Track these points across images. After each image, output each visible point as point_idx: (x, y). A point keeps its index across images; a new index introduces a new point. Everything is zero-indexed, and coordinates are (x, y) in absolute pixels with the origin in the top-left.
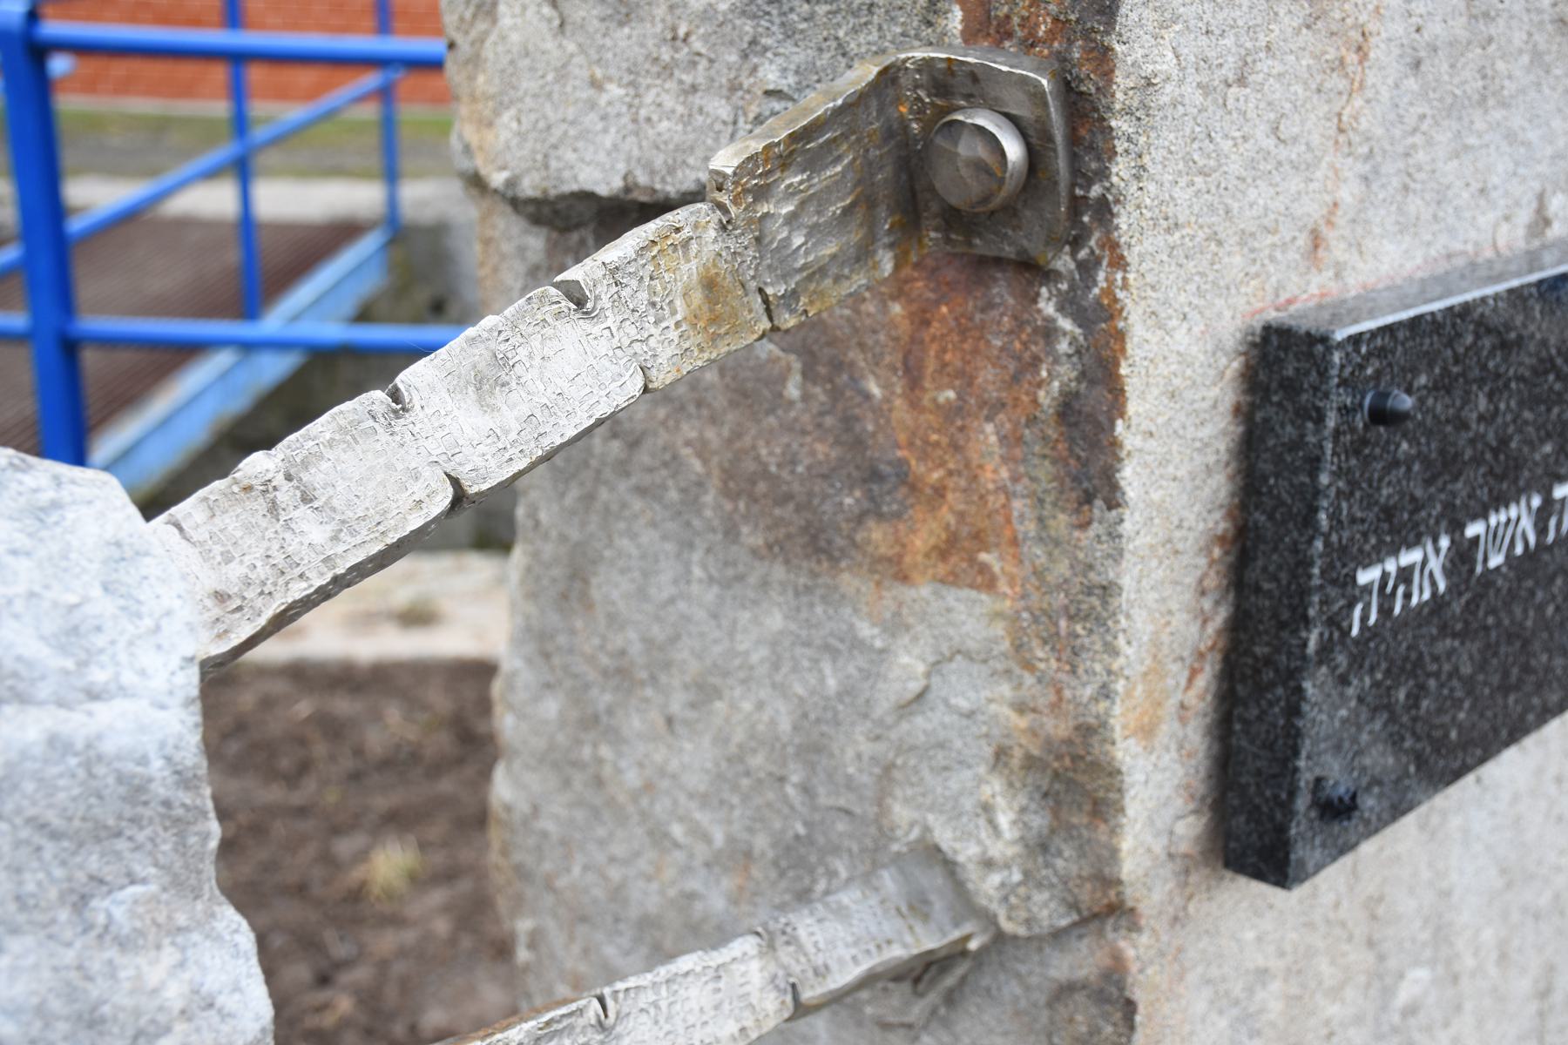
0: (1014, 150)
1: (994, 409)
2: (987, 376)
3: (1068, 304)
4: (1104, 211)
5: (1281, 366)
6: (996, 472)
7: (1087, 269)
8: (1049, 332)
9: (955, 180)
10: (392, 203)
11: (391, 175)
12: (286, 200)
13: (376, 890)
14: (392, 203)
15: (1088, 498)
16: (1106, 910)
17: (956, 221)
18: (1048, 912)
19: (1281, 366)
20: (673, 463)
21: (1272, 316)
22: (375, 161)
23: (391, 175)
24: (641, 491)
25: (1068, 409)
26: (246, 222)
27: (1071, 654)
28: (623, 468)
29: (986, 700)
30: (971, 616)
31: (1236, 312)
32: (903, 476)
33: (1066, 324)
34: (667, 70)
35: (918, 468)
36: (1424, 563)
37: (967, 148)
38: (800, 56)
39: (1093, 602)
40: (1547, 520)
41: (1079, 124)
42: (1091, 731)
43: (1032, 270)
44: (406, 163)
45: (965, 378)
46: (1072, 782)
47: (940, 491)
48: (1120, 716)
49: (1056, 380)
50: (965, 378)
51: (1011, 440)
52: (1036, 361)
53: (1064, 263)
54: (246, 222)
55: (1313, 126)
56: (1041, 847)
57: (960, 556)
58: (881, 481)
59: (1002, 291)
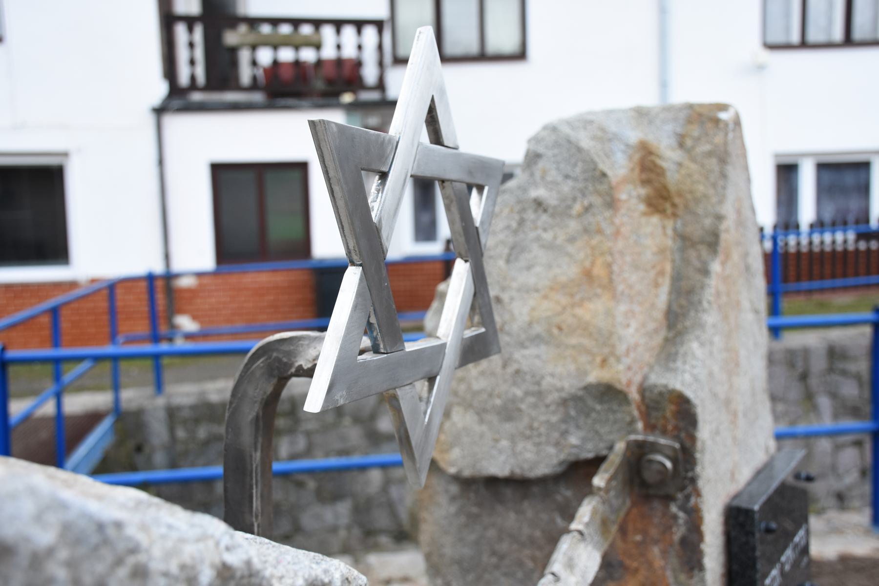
0: (669, 464)
1: (656, 542)
2: (654, 532)
3: (683, 508)
4: (693, 480)
6: (659, 563)
7: (687, 498)
8: (675, 517)
9: (650, 475)
10: (117, 401)
11: (116, 387)
12: (76, 404)
14: (117, 401)
15: (692, 569)
20: (520, 564)
22: (107, 380)
23: (116, 387)
24: (506, 575)
25: (684, 541)
26: (59, 415)
28: (497, 567)
32: (622, 565)
33: (681, 514)
34: (528, 438)
35: (628, 562)
37: (655, 467)
38: (581, 434)
40: (259, 358)
43: (668, 499)
44: (123, 380)
45: (645, 533)
47: (636, 570)
49: (679, 532)
50: (645, 533)
51: (664, 553)
52: (671, 527)
53: (680, 496)
54: (59, 415)
59: (657, 505)
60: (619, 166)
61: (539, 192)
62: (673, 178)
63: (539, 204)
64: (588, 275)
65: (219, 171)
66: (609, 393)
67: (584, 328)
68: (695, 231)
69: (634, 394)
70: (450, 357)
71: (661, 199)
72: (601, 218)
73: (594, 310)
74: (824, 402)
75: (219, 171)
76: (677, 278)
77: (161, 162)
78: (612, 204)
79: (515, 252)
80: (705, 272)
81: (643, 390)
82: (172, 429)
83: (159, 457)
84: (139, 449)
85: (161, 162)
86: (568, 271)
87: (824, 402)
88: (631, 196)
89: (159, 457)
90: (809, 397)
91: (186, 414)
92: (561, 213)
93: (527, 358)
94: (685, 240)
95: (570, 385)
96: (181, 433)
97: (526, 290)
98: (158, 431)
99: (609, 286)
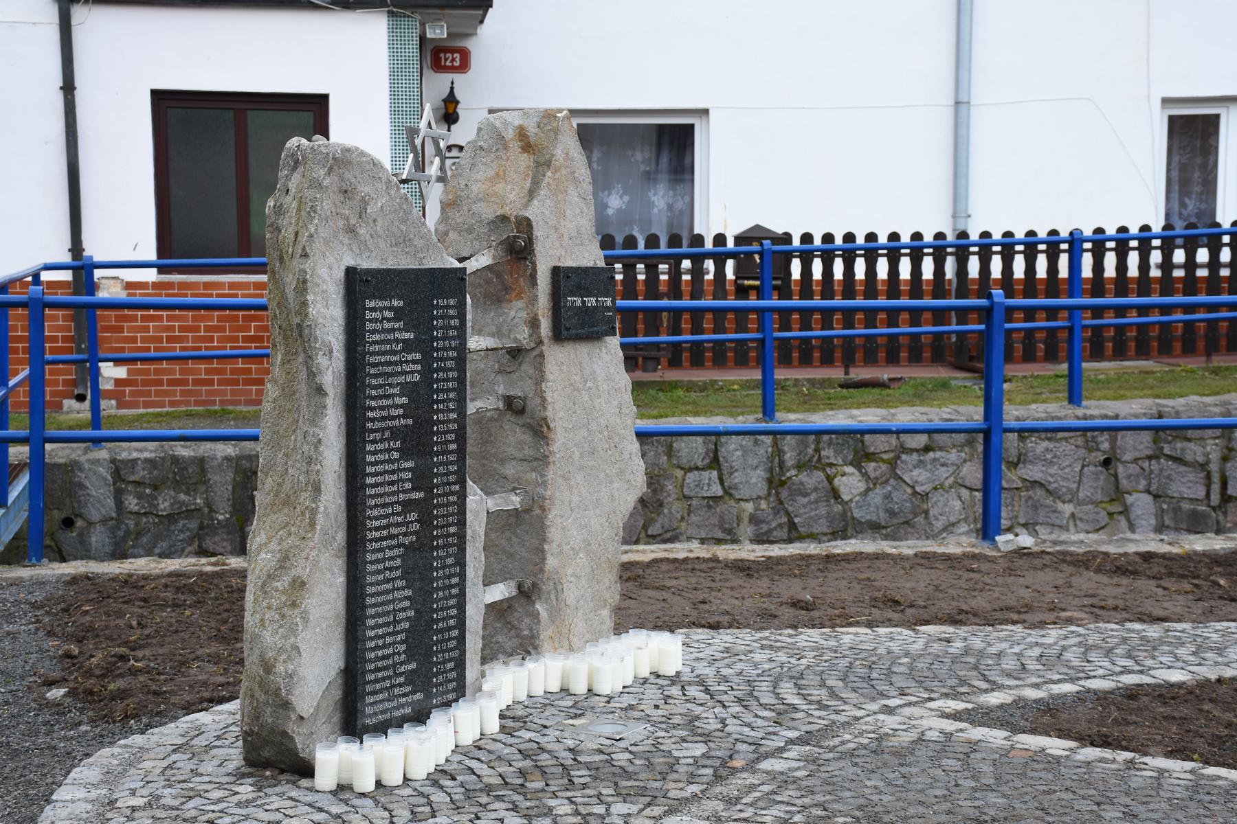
5: (556, 271)
13: (664, 177)
16: (541, 343)
17: (517, 253)
18: (533, 345)
19: (556, 271)
21: (423, 728)
27: (533, 305)
29: (523, 315)
30: (521, 304)
31: (551, 264)
36: (578, 301)
39: (535, 298)
41: (530, 241)
42: (536, 314)
43: (525, 259)
46: (534, 323)
48: (540, 313)
49: (529, 272)
55: (557, 244)
56: (531, 336)
57: (519, 297)
58: (507, 289)
60: (510, 134)
61: (481, 143)
62: (532, 139)
63: (481, 147)
64: (497, 174)
65: (163, 100)
66: (504, 219)
67: (496, 194)
68: (542, 160)
69: (513, 218)
70: (434, 179)
71: (527, 147)
72: (502, 153)
73: (499, 188)
74: (1141, 504)
75: (163, 100)
76: (534, 178)
77: (68, 87)
78: (506, 148)
79: (473, 166)
80: (544, 176)
81: (516, 217)
82: (118, 495)
83: (98, 537)
84: (68, 523)
85: (68, 87)
86: (491, 173)
87: (1141, 504)
88: (515, 146)
89: (98, 537)
90: (1117, 494)
91: (140, 474)
92: (488, 151)
93: (477, 208)
94: (538, 164)
95: (491, 216)
96: (132, 503)
97: (477, 181)
98: (98, 498)
99: (505, 178)
